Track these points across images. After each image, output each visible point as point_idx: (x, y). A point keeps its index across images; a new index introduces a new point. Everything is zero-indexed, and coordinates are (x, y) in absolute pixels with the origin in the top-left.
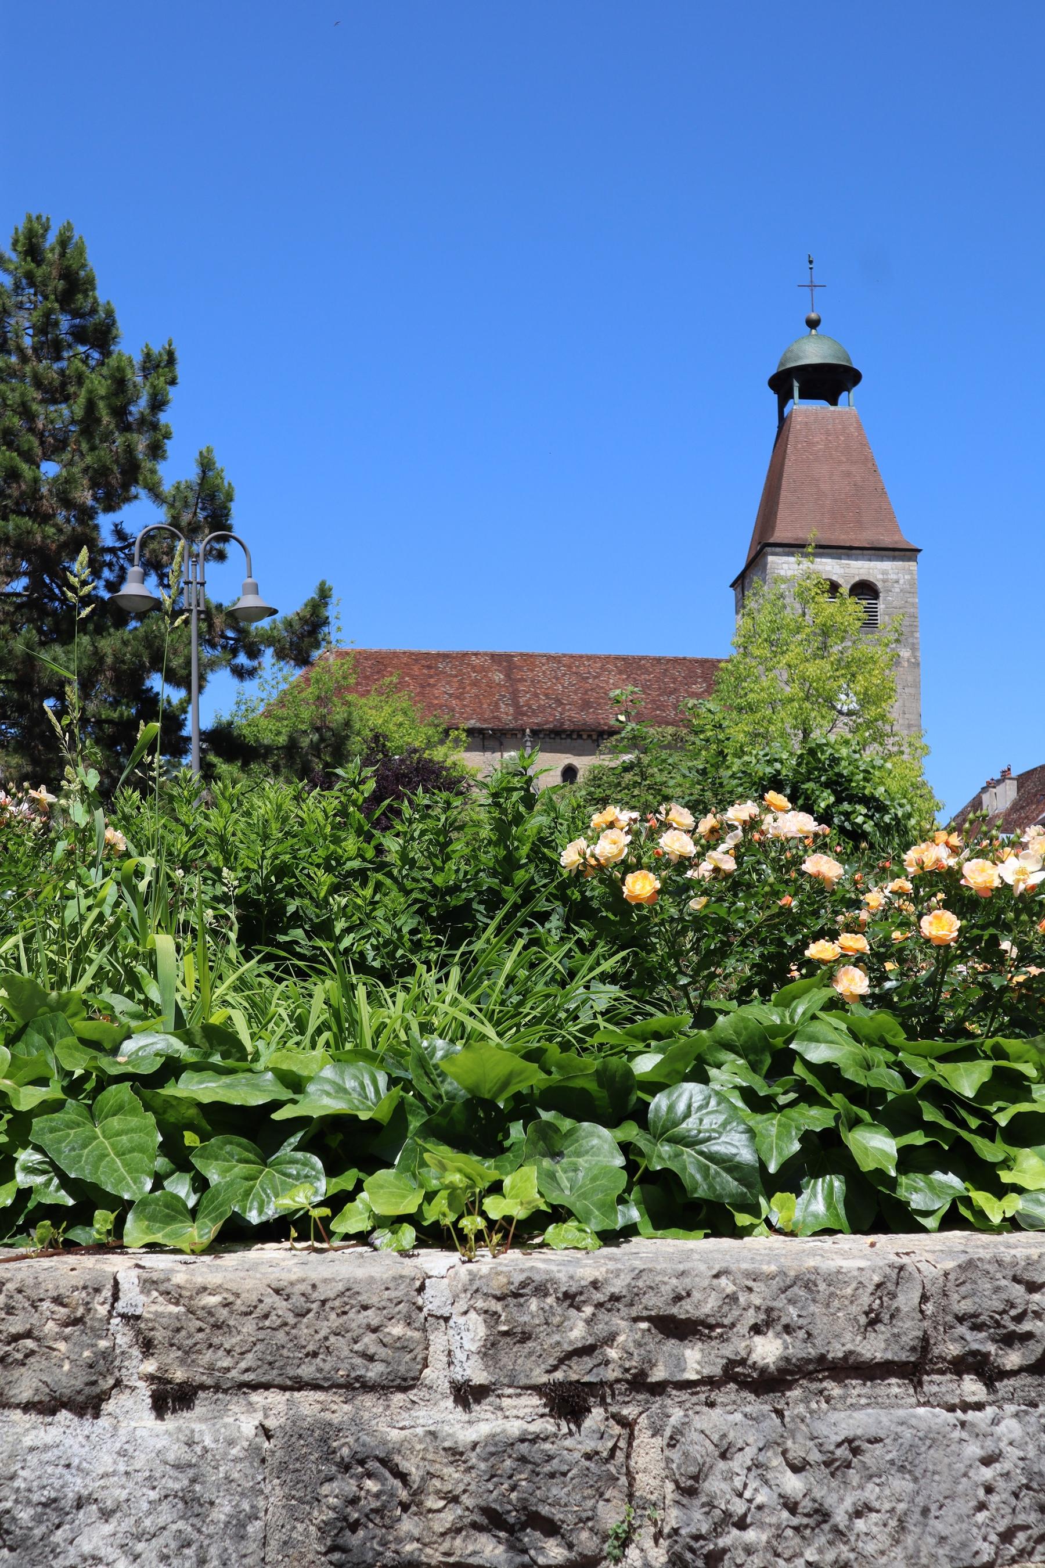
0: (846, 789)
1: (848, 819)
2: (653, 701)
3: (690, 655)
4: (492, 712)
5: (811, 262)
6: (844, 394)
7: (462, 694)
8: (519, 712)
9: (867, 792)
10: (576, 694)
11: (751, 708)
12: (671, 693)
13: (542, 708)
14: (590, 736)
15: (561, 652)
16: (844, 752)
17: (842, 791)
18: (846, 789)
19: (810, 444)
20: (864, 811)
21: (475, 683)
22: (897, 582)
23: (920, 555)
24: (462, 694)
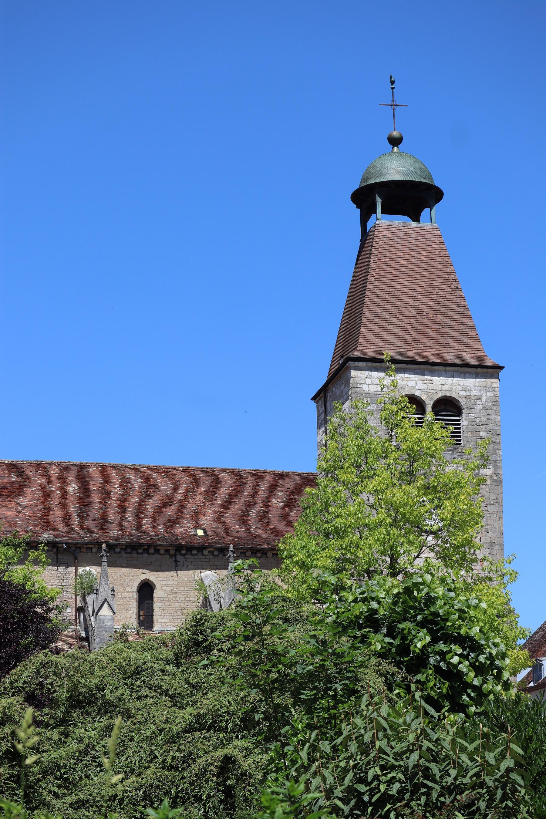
0: (442, 628)
1: (443, 659)
2: (233, 516)
3: (272, 467)
4: (67, 524)
5: (392, 82)
6: (427, 211)
7: (36, 505)
8: (94, 525)
9: (462, 632)
10: (153, 506)
11: (339, 533)
12: (251, 507)
13: (118, 521)
14: (167, 551)
15: (138, 463)
16: (440, 591)
17: (438, 631)
18: (442, 628)
19: (393, 259)
20: (459, 651)
21: (49, 495)
22: (480, 399)
23: (502, 373)
24: (36, 505)
